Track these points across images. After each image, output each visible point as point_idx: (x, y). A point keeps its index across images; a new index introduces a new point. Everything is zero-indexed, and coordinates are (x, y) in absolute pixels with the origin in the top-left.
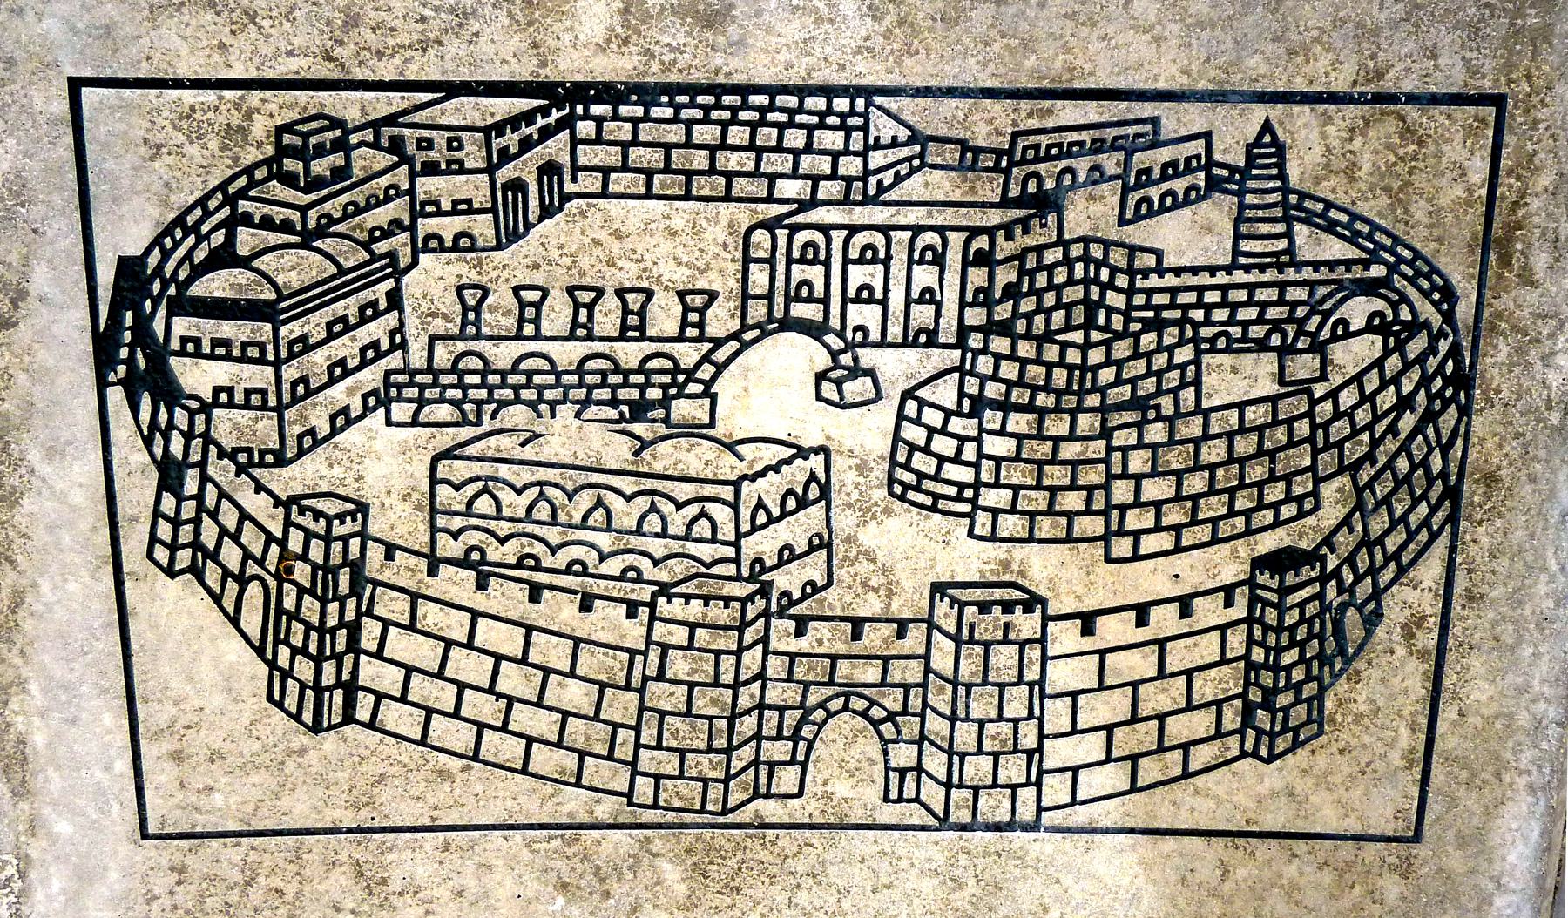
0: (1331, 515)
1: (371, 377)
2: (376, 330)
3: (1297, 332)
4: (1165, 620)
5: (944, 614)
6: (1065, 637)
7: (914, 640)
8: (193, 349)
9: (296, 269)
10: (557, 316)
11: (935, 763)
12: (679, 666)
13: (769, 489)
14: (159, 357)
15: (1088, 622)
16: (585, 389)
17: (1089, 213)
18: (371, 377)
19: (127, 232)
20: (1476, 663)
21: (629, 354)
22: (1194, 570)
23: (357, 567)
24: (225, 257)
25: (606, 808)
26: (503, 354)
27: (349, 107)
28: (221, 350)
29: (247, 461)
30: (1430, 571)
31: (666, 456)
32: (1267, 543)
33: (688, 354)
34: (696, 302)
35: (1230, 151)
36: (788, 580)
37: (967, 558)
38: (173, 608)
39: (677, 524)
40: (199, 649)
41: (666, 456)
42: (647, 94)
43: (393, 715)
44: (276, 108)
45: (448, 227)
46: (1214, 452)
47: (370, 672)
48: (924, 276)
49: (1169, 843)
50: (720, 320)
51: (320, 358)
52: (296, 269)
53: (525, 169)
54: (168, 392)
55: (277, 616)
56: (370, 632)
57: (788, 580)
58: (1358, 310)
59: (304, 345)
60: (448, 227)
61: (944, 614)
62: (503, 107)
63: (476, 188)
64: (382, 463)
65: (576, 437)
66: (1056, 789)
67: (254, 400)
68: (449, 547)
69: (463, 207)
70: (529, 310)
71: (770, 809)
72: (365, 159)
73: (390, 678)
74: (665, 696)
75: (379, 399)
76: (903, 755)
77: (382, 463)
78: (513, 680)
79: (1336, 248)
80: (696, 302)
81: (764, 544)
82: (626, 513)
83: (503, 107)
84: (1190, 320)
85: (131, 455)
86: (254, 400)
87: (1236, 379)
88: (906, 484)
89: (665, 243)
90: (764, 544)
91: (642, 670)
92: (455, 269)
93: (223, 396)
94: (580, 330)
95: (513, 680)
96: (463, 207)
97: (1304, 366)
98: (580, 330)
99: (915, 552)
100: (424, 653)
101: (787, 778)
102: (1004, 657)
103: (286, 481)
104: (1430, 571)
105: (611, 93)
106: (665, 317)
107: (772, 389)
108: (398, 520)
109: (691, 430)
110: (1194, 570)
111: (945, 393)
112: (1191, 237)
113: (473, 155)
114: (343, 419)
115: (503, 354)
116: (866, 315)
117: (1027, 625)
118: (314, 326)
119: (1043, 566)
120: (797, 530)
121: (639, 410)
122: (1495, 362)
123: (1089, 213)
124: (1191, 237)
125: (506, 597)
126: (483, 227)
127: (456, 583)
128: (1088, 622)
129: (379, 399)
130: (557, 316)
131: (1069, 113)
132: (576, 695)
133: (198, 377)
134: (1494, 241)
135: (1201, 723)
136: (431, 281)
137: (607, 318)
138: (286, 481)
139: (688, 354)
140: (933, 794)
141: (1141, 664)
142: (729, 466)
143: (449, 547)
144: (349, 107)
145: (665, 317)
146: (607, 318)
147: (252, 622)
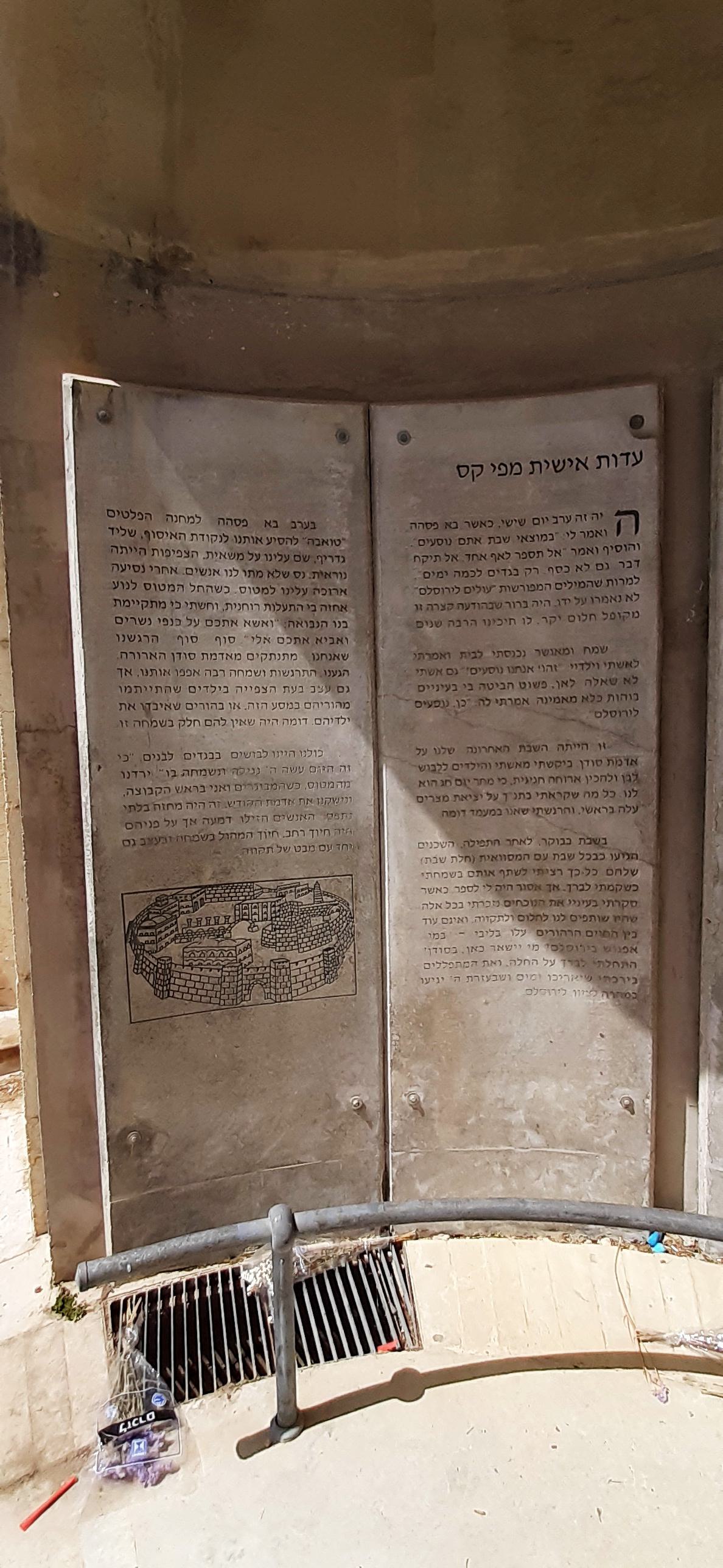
0: (334, 941)
1: (172, 936)
2: (173, 928)
3: (324, 912)
4: (309, 962)
5: (272, 965)
6: (293, 966)
7: (268, 970)
8: (141, 935)
9: (158, 920)
10: (204, 922)
11: (273, 991)
12: (227, 979)
13: (241, 947)
14: (135, 936)
15: (297, 963)
16: (208, 933)
17: (289, 897)
18: (172, 936)
19: (130, 917)
20: (362, 964)
21: (216, 927)
22: (312, 953)
23: (170, 969)
24: (147, 919)
25: (216, 1007)
26: (195, 930)
27: (168, 893)
28: (147, 935)
29: (150, 953)
30: (352, 949)
31: (223, 944)
32: (325, 947)
33: (226, 926)
34: (227, 918)
35: (311, 886)
36: (245, 962)
37: (276, 955)
38: (137, 980)
39: (226, 954)
40: (141, 985)
41: (223, 944)
42: (217, 886)
43: (176, 995)
44: (156, 894)
45: (185, 910)
46: (314, 933)
47: (173, 987)
48: (265, 910)
49: (480, 1196)
50: (231, 920)
51: (163, 934)
52: (158, 920)
53: (197, 899)
54: (136, 942)
55: (156, 979)
56: (172, 981)
57: (245, 962)
58: (334, 908)
59: (161, 932)
60: (185, 910)
61: (272, 965)
62: (194, 890)
63: (190, 903)
64: (174, 950)
65: (206, 942)
66: (294, 993)
67: (152, 942)
68: (186, 963)
69: (187, 906)
70: (199, 922)
71: (244, 1003)
72: (171, 901)
73: (175, 988)
74: (225, 985)
75: (174, 940)
76: (267, 990)
77: (174, 950)
78: (198, 985)
79: (329, 899)
80: (227, 918)
81: (241, 956)
82: (217, 954)
83: (194, 890)
84: (310, 913)
85: (131, 954)
86: (152, 942)
87: (317, 921)
88: (264, 944)
89: (221, 909)
90: (241, 956)
91: (221, 980)
92: (187, 916)
93: (147, 942)
94: (217, 923)
95: (198, 985)
96: (187, 906)
97: (327, 918)
98: (217, 923)
99: (268, 954)
100: (182, 982)
101: (247, 997)
102: (283, 971)
103: (158, 955)
104: (352, 949)
105: (210, 886)
106: (222, 920)
107: (240, 931)
108: (176, 960)
109: (227, 938)
110: (312, 953)
111: (270, 928)
112: (306, 900)
113: (189, 898)
114: (167, 943)
115: (195, 930)
116: (255, 917)
117: (286, 965)
118: (163, 929)
119: (288, 955)
120: (246, 953)
121: (218, 936)
122: (357, 914)
123: (289, 897)
124: (306, 900)
125: (196, 971)
126: (191, 909)
127: (187, 969)
128: (297, 963)
129: (174, 940)
130: (204, 922)
131: (286, 882)
132: (209, 987)
133: (142, 940)
134: (354, 897)
135: (318, 978)
136: (182, 919)
137: (212, 922)
138: (158, 955)
139: (226, 926)
140: (273, 997)
141: (306, 969)
142: (234, 944)
143: (186, 963)
144: (168, 893)
145: (222, 920)
146: (212, 922)
147: (151, 981)
